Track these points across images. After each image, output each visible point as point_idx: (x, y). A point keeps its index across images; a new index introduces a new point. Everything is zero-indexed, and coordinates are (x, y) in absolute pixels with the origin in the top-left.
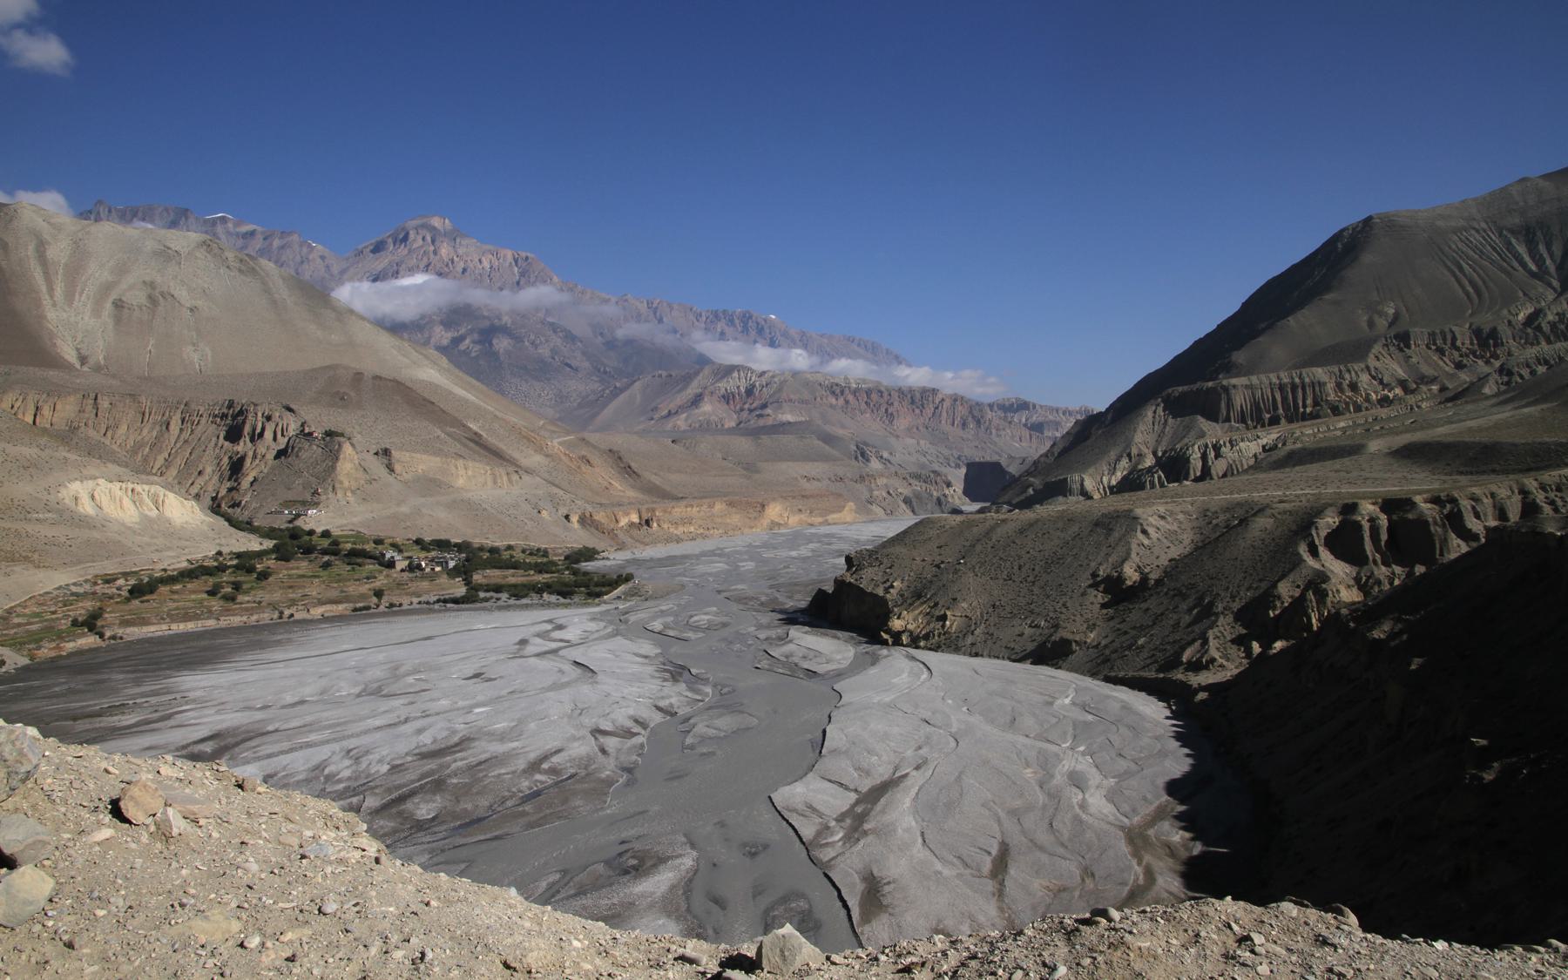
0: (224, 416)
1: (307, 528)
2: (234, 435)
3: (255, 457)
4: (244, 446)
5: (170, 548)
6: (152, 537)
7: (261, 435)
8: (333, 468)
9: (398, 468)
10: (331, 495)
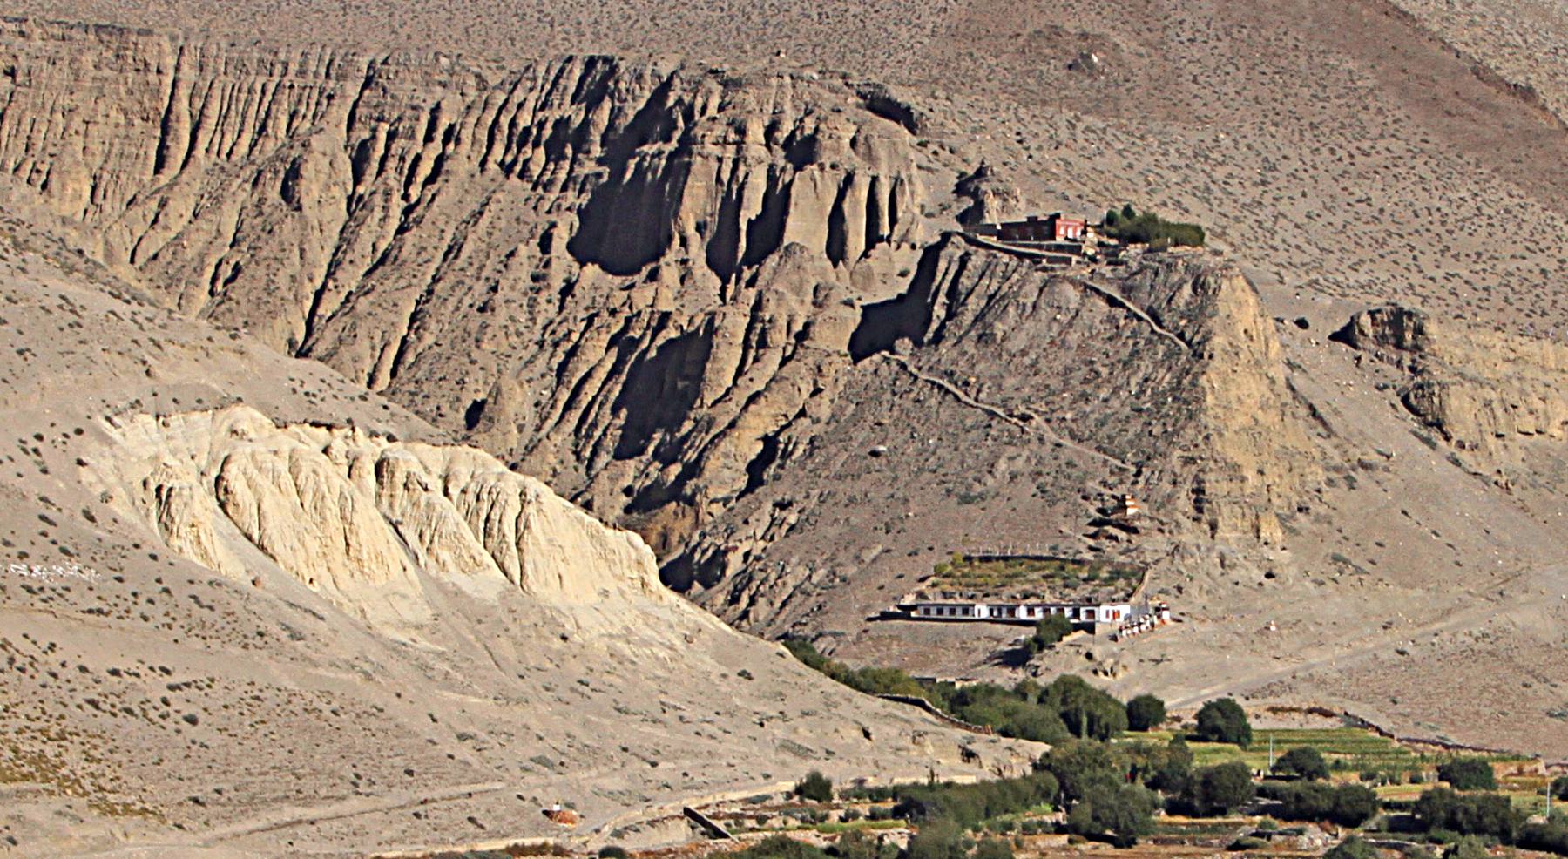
0: (564, 140)
1: (1124, 687)
2: (622, 231)
3: (756, 340)
4: (681, 290)
5: (592, 754)
6: (503, 697)
7: (769, 233)
8: (1184, 397)
9: (1460, 407)
10: (1190, 535)
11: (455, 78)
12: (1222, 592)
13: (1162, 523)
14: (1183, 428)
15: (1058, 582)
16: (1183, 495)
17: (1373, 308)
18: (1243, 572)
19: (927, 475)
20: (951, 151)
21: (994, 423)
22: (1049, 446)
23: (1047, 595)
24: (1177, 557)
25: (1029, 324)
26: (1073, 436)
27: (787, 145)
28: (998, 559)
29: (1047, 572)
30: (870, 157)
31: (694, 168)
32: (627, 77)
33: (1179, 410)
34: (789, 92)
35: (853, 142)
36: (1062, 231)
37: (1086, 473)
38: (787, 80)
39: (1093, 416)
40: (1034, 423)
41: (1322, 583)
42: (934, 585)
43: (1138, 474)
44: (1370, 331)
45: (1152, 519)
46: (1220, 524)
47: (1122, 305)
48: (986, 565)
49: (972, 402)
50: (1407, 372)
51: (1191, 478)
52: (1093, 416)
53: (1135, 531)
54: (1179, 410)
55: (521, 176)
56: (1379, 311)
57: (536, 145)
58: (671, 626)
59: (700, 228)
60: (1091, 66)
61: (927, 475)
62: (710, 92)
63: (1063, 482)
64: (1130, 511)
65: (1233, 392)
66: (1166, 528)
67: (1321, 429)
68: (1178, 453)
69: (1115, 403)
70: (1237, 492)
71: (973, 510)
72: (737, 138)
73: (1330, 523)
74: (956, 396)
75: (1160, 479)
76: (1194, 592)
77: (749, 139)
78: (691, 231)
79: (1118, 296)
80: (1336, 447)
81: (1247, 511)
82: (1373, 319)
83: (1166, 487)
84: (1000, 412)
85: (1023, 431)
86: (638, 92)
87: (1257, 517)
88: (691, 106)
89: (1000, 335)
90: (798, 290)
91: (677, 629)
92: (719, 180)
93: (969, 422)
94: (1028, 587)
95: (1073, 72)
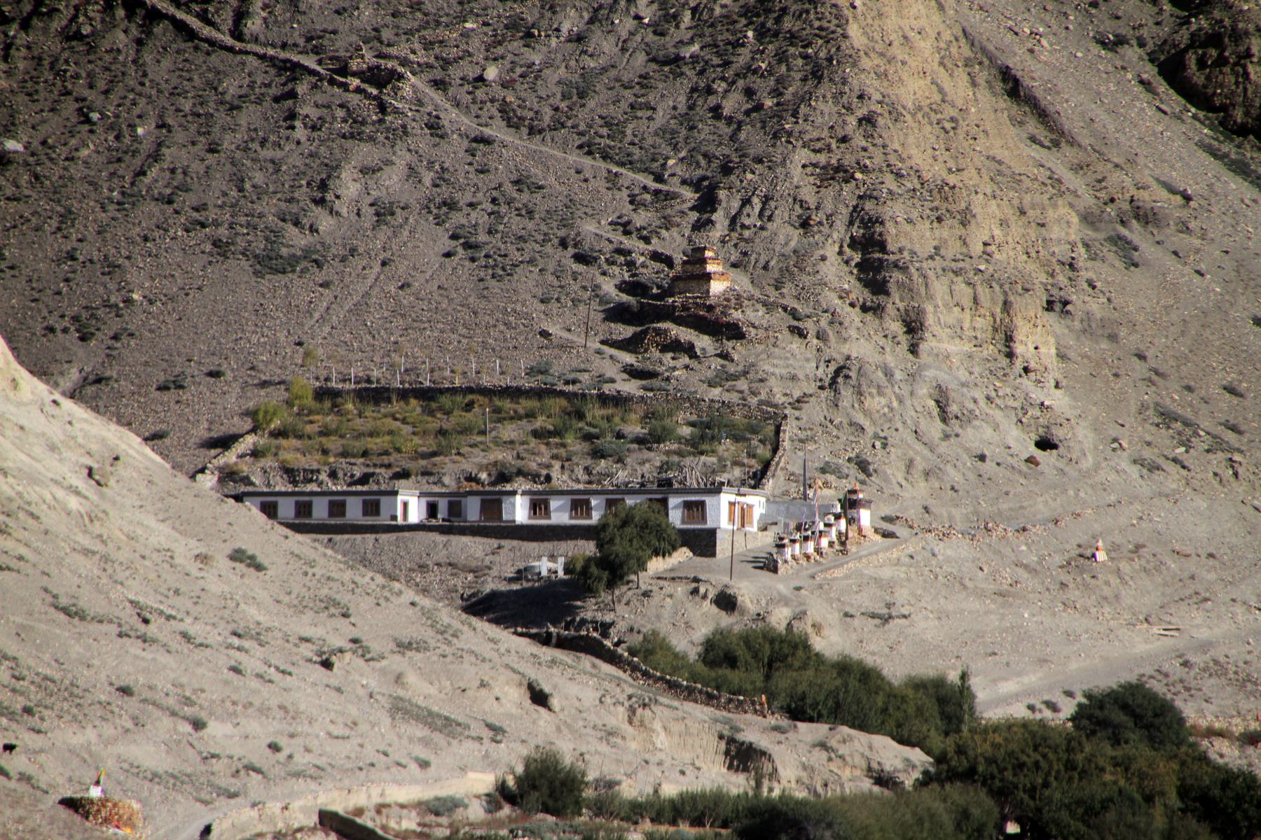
10: (865, 342)
12: (954, 475)
13: (794, 314)
14: (805, 98)
15: (575, 445)
16: (831, 251)
18: (988, 432)
19: (149, 211)
21: (302, 88)
22: (458, 145)
23: (555, 473)
24: (847, 394)
26: (513, 122)
28: (404, 395)
29: (540, 422)
33: (781, 57)
37: (571, 203)
39: (553, 76)
40: (407, 90)
41: (1154, 468)
42: (256, 454)
43: (707, 203)
45: (769, 306)
46: (930, 320)
48: (373, 417)
49: (229, 41)
51: (845, 212)
52: (553, 76)
53: (735, 332)
54: (781, 57)
58: (53, 448)
61: (149, 211)
63: (516, 224)
64: (717, 287)
65: (892, 23)
66: (809, 325)
67: (1033, 126)
69: (604, 45)
70: (954, 248)
71: (300, 287)
73: (1113, 338)
74: (180, 26)
75: (766, 215)
76: (896, 473)
80: (1078, 168)
81: (984, 293)
83: (785, 235)
84: (310, 62)
85: (382, 108)
87: (1007, 305)
91: (67, 454)
93: (231, 87)
94: (503, 456)
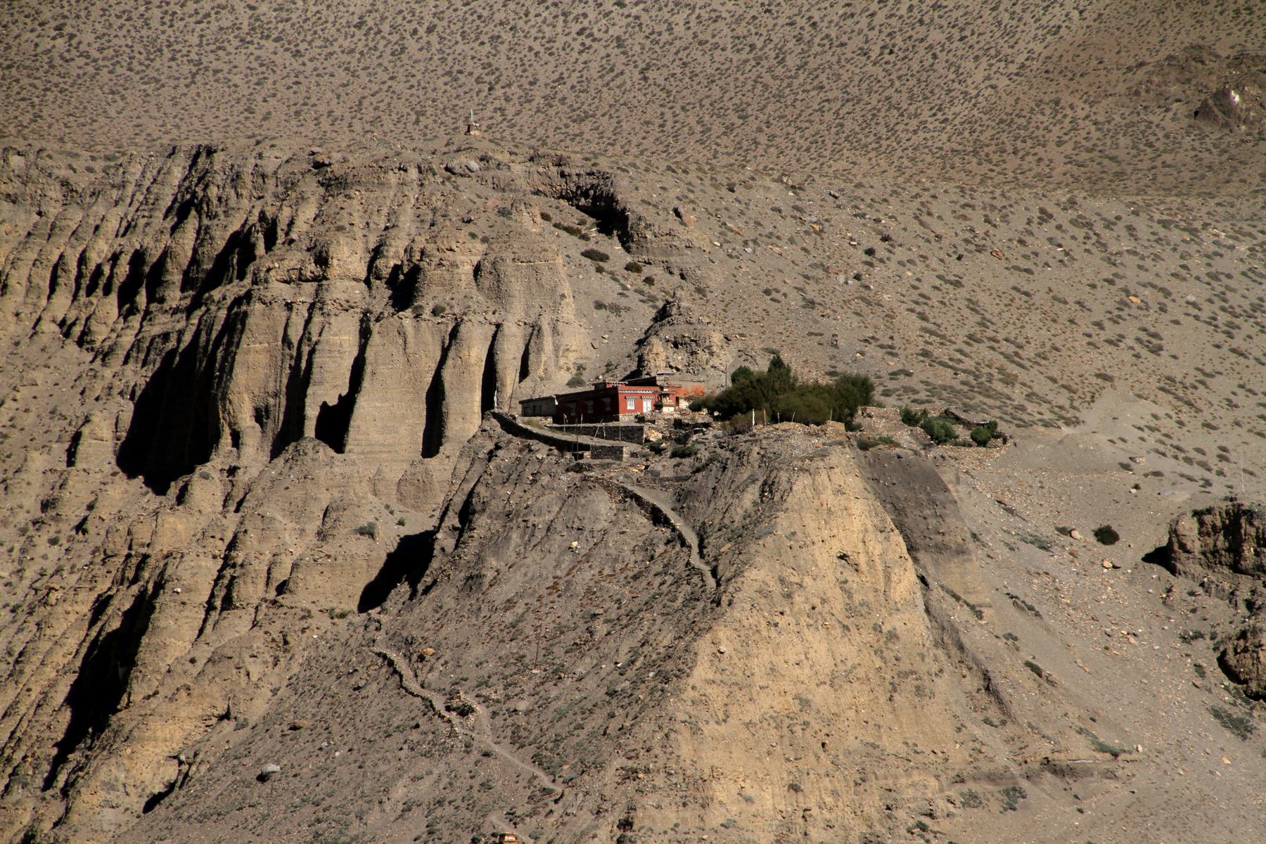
11: (30, 188)
17: (1200, 507)
20: (682, 276)
25: (534, 556)
27: (392, 282)
30: (499, 294)
31: (251, 321)
32: (219, 179)
34: (413, 194)
35: (477, 270)
36: (631, 406)
38: (413, 173)
44: (1195, 544)
47: (666, 522)
50: (1243, 610)
55: (80, 342)
56: (1209, 511)
57: (107, 291)
59: (261, 415)
60: (1228, 110)
62: (302, 198)
67: (994, 713)
68: (619, 761)
72: (318, 271)
77: (335, 269)
78: (246, 420)
79: (666, 510)
82: (1202, 523)
83: (586, 819)
86: (233, 202)
88: (274, 222)
89: (490, 575)
90: (297, 513)
92: (286, 340)
95: (1200, 123)
